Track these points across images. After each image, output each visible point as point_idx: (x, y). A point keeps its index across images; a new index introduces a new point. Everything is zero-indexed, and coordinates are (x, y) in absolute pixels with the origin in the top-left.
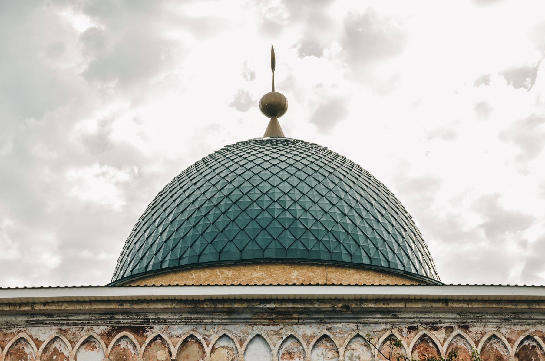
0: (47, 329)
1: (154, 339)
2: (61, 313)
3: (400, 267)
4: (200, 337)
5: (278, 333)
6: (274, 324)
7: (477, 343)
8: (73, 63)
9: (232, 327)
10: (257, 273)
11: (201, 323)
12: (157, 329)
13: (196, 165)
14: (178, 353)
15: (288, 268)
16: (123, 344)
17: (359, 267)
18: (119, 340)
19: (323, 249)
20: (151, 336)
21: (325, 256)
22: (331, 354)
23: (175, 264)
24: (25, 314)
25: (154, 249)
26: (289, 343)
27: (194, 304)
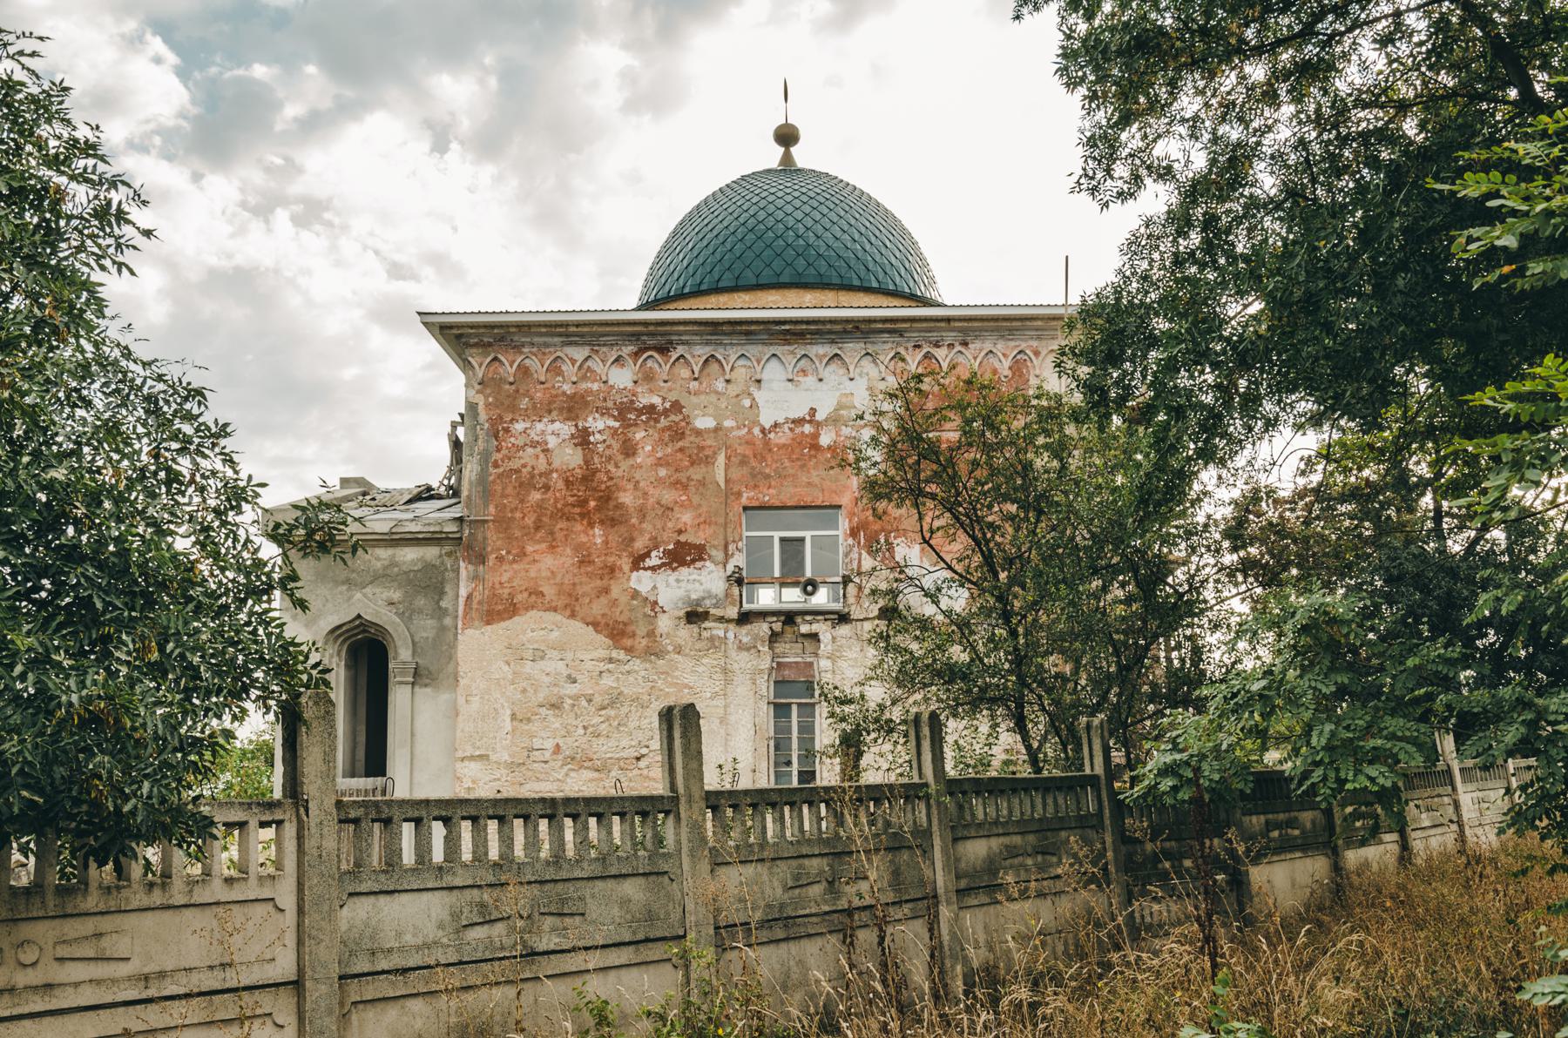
0: (580, 349)
2: (592, 335)
5: (792, 353)
8: (607, 100)
10: (772, 297)
12: (680, 350)
14: (701, 371)
15: (802, 292)
16: (650, 363)
20: (674, 356)
21: (836, 281)
22: (842, 371)
24: (560, 335)
25: (676, 275)
26: (803, 362)
27: (714, 325)
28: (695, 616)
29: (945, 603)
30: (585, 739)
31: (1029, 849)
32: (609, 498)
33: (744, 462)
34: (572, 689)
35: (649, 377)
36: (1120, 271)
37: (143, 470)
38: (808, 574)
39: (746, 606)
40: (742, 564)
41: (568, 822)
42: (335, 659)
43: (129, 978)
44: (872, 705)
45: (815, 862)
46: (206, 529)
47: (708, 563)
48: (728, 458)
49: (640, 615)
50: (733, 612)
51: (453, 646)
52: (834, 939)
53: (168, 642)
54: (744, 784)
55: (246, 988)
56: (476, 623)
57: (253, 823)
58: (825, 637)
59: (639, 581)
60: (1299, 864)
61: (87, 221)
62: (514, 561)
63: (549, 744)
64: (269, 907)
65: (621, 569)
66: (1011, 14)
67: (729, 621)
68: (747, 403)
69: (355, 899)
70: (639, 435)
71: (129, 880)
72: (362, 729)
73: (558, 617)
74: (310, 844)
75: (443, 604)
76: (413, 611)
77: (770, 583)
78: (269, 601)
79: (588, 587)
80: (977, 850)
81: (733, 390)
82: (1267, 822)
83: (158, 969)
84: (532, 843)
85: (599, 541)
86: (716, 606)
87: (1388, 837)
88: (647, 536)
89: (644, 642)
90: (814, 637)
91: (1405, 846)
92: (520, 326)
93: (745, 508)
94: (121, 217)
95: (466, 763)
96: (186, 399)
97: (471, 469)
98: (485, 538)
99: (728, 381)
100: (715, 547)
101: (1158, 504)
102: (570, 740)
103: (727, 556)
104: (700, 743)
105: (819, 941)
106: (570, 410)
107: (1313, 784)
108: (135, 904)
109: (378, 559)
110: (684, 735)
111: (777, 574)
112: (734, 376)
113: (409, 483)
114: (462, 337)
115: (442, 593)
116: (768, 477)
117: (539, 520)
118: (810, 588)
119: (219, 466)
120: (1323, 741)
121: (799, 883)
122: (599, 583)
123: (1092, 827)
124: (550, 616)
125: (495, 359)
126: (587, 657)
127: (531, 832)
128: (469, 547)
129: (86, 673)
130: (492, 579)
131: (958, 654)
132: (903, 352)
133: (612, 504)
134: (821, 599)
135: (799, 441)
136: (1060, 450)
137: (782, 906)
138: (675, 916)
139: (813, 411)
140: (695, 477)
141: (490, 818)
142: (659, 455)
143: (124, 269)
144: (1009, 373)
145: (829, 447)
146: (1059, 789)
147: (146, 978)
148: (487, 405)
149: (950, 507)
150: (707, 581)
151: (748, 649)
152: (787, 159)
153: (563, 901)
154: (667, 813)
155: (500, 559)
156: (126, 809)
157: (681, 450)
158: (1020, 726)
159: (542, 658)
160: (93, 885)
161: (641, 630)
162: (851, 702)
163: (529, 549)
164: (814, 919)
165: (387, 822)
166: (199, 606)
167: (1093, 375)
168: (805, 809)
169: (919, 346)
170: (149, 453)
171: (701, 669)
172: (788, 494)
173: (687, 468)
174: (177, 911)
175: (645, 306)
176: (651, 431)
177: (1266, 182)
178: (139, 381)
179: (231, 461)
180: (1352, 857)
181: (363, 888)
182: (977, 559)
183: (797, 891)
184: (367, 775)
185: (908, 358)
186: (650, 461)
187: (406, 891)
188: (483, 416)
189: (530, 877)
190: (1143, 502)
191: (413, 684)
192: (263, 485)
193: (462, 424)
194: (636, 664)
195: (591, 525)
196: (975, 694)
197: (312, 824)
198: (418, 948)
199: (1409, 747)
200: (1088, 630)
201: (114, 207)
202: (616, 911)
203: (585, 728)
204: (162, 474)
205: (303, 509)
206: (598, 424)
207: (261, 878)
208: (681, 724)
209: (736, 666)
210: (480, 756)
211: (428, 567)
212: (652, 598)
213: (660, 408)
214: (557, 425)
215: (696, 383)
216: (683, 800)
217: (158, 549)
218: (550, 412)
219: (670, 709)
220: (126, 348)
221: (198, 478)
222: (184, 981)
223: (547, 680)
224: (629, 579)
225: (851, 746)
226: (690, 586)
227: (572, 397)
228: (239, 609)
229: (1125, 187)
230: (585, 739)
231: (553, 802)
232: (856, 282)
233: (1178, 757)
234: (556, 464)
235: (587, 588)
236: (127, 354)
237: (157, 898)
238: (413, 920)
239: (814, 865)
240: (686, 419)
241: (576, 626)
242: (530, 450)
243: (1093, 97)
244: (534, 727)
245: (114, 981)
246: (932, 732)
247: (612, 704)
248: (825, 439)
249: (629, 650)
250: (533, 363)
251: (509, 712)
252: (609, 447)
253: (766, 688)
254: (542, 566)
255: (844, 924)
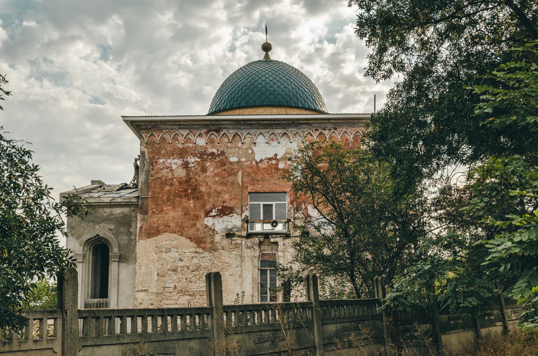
0: (185, 130)
1: (223, 135)
2: (190, 125)
3: (313, 108)
4: (240, 134)
5: (268, 132)
6: (267, 129)
7: (339, 134)
9: (251, 130)
10: (261, 110)
11: (240, 129)
12: (224, 131)
13: (238, 70)
14: (232, 139)
15: (272, 108)
16: (212, 136)
17: (298, 107)
18: (211, 135)
19: (285, 101)
22: (287, 139)
23: (231, 107)
24: (177, 125)
25: (223, 101)
26: (272, 136)
28: (229, 235)
29: (323, 231)
30: (186, 283)
31: (353, 328)
32: (196, 189)
33: (249, 175)
34: (181, 264)
36: (387, 105)
38: (274, 218)
39: (250, 231)
42: (88, 252)
44: (295, 271)
45: (267, 333)
46: (29, 206)
47: (235, 214)
48: (243, 173)
49: (208, 235)
50: (244, 234)
51: (135, 246)
53: (11, 250)
54: (247, 301)
56: (144, 238)
58: (281, 243)
59: (208, 221)
62: (159, 213)
63: (172, 285)
64: (51, 351)
65: (200, 216)
67: (243, 237)
68: (250, 152)
69: (85, 348)
72: (99, 279)
74: (67, 327)
75: (131, 230)
77: (260, 221)
78: (53, 233)
79: (188, 224)
80: (331, 328)
81: (245, 147)
82: (449, 318)
84: (155, 325)
85: (192, 205)
86: (238, 231)
87: (498, 324)
88: (211, 204)
89: (210, 245)
90: (276, 243)
91: (505, 327)
92: (161, 121)
93: (249, 193)
95: (139, 293)
96: (23, 155)
98: (147, 204)
99: (243, 143)
100: (237, 208)
103: (242, 212)
104: (221, 287)
106: (181, 154)
109: (105, 212)
110: (215, 284)
111: (262, 219)
112: (245, 141)
113: (119, 182)
114: (138, 126)
115: (130, 226)
116: (258, 180)
118: (274, 224)
121: (260, 341)
122: (192, 222)
123: (378, 319)
124: (172, 235)
125: (152, 134)
126: (187, 251)
127: (154, 322)
128: (141, 208)
130: (150, 220)
131: (326, 251)
133: (197, 191)
134: (280, 228)
135: (270, 167)
137: (253, 350)
139: (276, 155)
140: (230, 181)
141: (138, 316)
142: (216, 172)
145: (282, 170)
146: (365, 304)
148: (149, 152)
149: (325, 194)
150: (234, 221)
151: (250, 248)
152: (267, 56)
154: (208, 314)
155: (153, 213)
157: (224, 170)
158: (353, 281)
159: (169, 251)
161: (209, 241)
162: (287, 270)
163: (165, 209)
167: (376, 145)
168: (263, 312)
170: (7, 177)
171: (231, 256)
172: (267, 187)
174: (15, 353)
178: (5, 148)
179: (39, 180)
181: (88, 344)
183: (259, 345)
185: (313, 135)
186: (212, 174)
187: (105, 345)
188: (147, 157)
189: (153, 339)
191: (119, 262)
192: (51, 189)
193: (139, 159)
194: (206, 254)
195: (189, 199)
196: (332, 266)
203: (186, 279)
204: (12, 185)
205: (67, 198)
206: (192, 160)
207: (47, 340)
208: (214, 280)
209: (245, 255)
210: (145, 290)
211: (125, 216)
212: (213, 228)
213: (216, 154)
214: (176, 160)
215: (230, 144)
216: (214, 309)
217: (9, 214)
218: (173, 155)
219: (210, 274)
221: (26, 187)
223: (171, 260)
224: (204, 220)
225: (287, 288)
226: (228, 223)
227: (182, 149)
228: (42, 236)
229: (386, 74)
230: (186, 283)
232: (293, 105)
233: (398, 294)
234: (176, 175)
235: (187, 224)
237: (7, 348)
240: (227, 158)
241: (183, 239)
242: (165, 170)
244: (166, 278)
247: (197, 269)
248: (281, 166)
249: (204, 249)
250: (167, 136)
251: (156, 273)
252: (196, 169)
253: (257, 263)
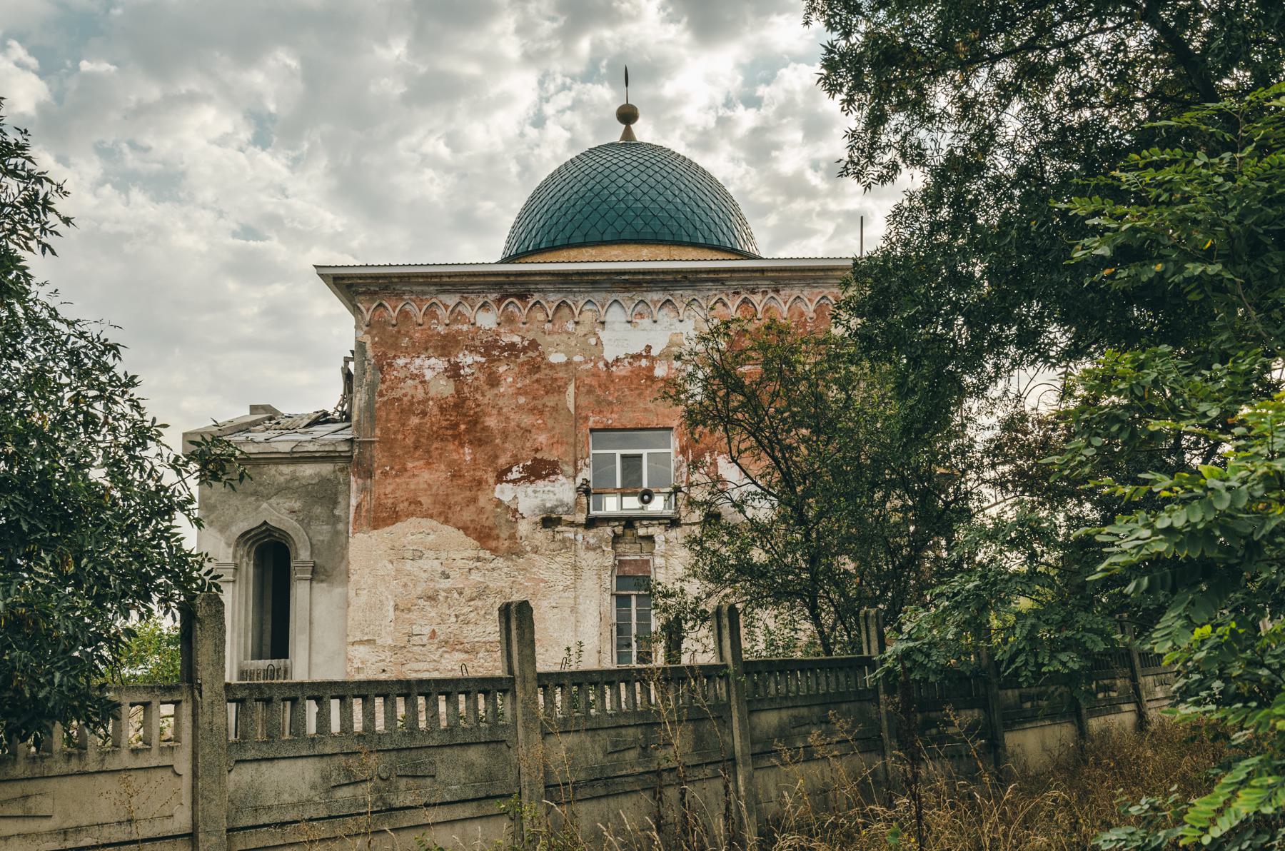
0: (452, 296)
2: (463, 284)
5: (631, 299)
10: (614, 252)
12: (537, 297)
14: (554, 314)
15: (639, 247)
16: (511, 308)
22: (673, 314)
24: (435, 284)
28: (549, 521)
29: (750, 513)
30: (456, 626)
31: (815, 720)
32: (476, 423)
33: (590, 391)
34: (446, 584)
35: (510, 320)
36: (887, 238)
37: (64, 414)
38: (645, 485)
39: (593, 513)
40: (589, 478)
41: (421, 700)
42: (245, 559)
43: (51, 833)
44: (690, 599)
45: (631, 731)
46: (117, 462)
47: (560, 477)
48: (577, 388)
49: (503, 521)
50: (581, 518)
52: (646, 796)
54: (589, 662)
55: (144, 841)
57: (155, 704)
59: (502, 492)
60: (1048, 731)
61: (19, 208)
62: (397, 476)
63: (427, 631)
64: (169, 773)
65: (487, 482)
66: (802, 21)
67: (578, 525)
68: (593, 341)
69: (241, 765)
70: (502, 369)
71: (51, 751)
72: (268, 618)
73: (434, 523)
74: (203, 720)
75: (337, 512)
76: (311, 518)
78: (170, 520)
80: (769, 720)
81: (581, 330)
82: (1020, 695)
83: (74, 824)
85: (468, 458)
86: (567, 513)
87: (1126, 707)
88: (509, 454)
89: (507, 543)
90: (650, 539)
93: (592, 430)
94: (47, 206)
95: (356, 647)
96: (103, 353)
97: (360, 398)
98: (372, 457)
99: (577, 323)
100: (566, 463)
101: (921, 431)
102: (443, 627)
103: (577, 471)
105: (634, 798)
106: (443, 347)
107: (1017, 668)
108: (56, 771)
109: (281, 474)
110: (519, 627)
111: (619, 485)
112: (582, 318)
113: (309, 409)
114: (350, 285)
116: (610, 403)
117: (417, 440)
118: (646, 497)
119: (127, 410)
120: (1025, 632)
121: (618, 748)
122: (468, 493)
123: (869, 700)
125: (381, 305)
126: (458, 556)
127: (389, 708)
128: (359, 464)
129: (11, 583)
130: (378, 490)
131: (758, 555)
132: (725, 299)
133: (479, 427)
135: (637, 373)
136: (846, 384)
137: (603, 768)
138: (512, 777)
139: (649, 348)
141: (355, 697)
142: (519, 385)
143: (47, 250)
144: (814, 315)
147: (65, 832)
148: (374, 344)
149: (755, 432)
150: (560, 491)
151: (594, 549)
152: (628, 134)
153: (417, 766)
155: (385, 474)
156: (41, 695)
157: (538, 381)
158: (815, 619)
159: (420, 557)
160: (21, 756)
161: (504, 534)
162: (673, 595)
163: (410, 465)
164: (630, 779)
165: (268, 701)
166: (109, 527)
168: (623, 686)
169: (738, 293)
171: (554, 566)
173: (543, 397)
175: (506, 261)
176: (512, 366)
177: (1001, 163)
178: (64, 338)
179: (138, 407)
180: (1095, 724)
181: (248, 756)
182: (777, 475)
183: (615, 756)
184: (272, 658)
185: (729, 304)
186: (510, 391)
188: (370, 353)
190: (906, 431)
191: (311, 580)
192: (165, 426)
193: (352, 359)
194: (500, 562)
195: (462, 445)
196: (771, 586)
197: (205, 704)
198: (294, 806)
199: (1095, 637)
200: (868, 539)
201: (41, 196)
202: (461, 773)
203: (457, 616)
204: (81, 417)
205: (199, 444)
206: (467, 359)
207: (161, 749)
208: (517, 618)
210: (368, 641)
211: (324, 481)
212: (513, 507)
213: (520, 346)
214: (433, 361)
215: (550, 325)
216: (518, 681)
217: (76, 480)
218: (427, 349)
219: (508, 605)
220: (53, 309)
221: (110, 421)
222: (97, 834)
223: (424, 575)
225: (674, 634)
226: (545, 496)
227: (445, 337)
230: (456, 626)
231: (408, 683)
232: (686, 239)
233: (911, 644)
234: (432, 393)
235: (458, 498)
236: (54, 314)
237: (75, 766)
238: (290, 781)
239: (630, 734)
241: (449, 531)
242: (410, 382)
243: (850, 101)
244: (413, 615)
245: (38, 835)
246: (730, 621)
247: (480, 596)
248: (660, 371)
249: (494, 551)
250: (412, 308)
251: (392, 603)
252: (476, 379)
253: (609, 581)
254: (421, 480)
255: (654, 782)
